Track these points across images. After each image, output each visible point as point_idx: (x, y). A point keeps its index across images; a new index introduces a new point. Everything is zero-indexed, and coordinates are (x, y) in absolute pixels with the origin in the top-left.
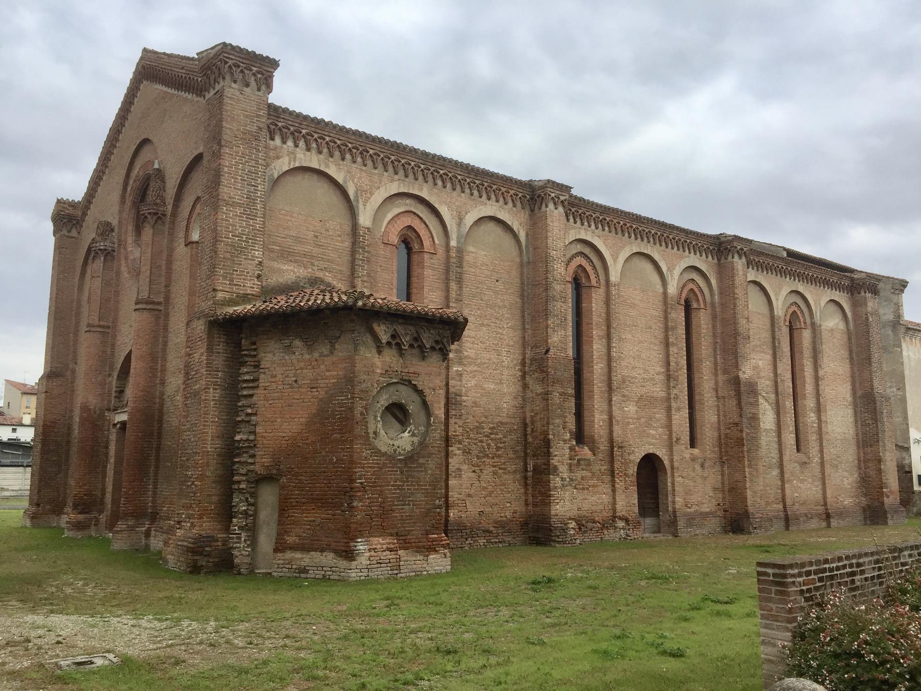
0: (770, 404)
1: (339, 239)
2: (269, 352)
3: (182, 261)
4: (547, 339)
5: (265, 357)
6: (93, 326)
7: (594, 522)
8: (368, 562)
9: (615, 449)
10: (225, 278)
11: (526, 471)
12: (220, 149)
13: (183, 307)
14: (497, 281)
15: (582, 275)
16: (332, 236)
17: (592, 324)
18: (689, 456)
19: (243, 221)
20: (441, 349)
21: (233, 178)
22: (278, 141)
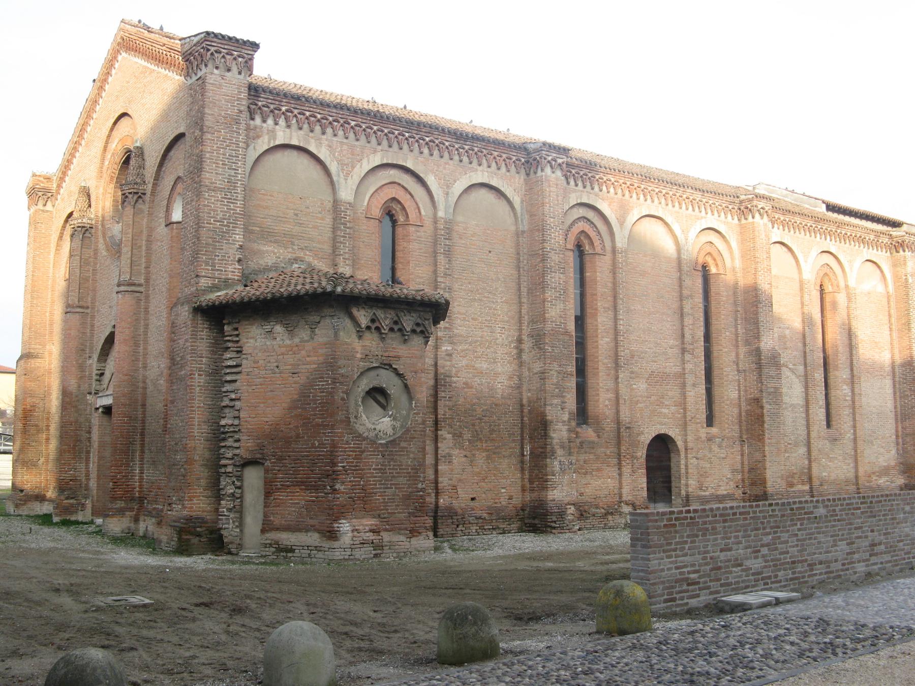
0: (798, 377)
1: (320, 215)
2: (251, 338)
3: (162, 242)
4: (544, 313)
5: (247, 342)
6: (73, 307)
7: (597, 507)
8: (352, 542)
9: (622, 430)
10: (207, 264)
11: (523, 455)
12: (202, 135)
13: (164, 289)
14: (490, 252)
15: (586, 242)
16: (312, 213)
17: (596, 295)
18: (705, 435)
19: (225, 205)
20: (422, 332)
21: (214, 163)
22: (258, 120)
